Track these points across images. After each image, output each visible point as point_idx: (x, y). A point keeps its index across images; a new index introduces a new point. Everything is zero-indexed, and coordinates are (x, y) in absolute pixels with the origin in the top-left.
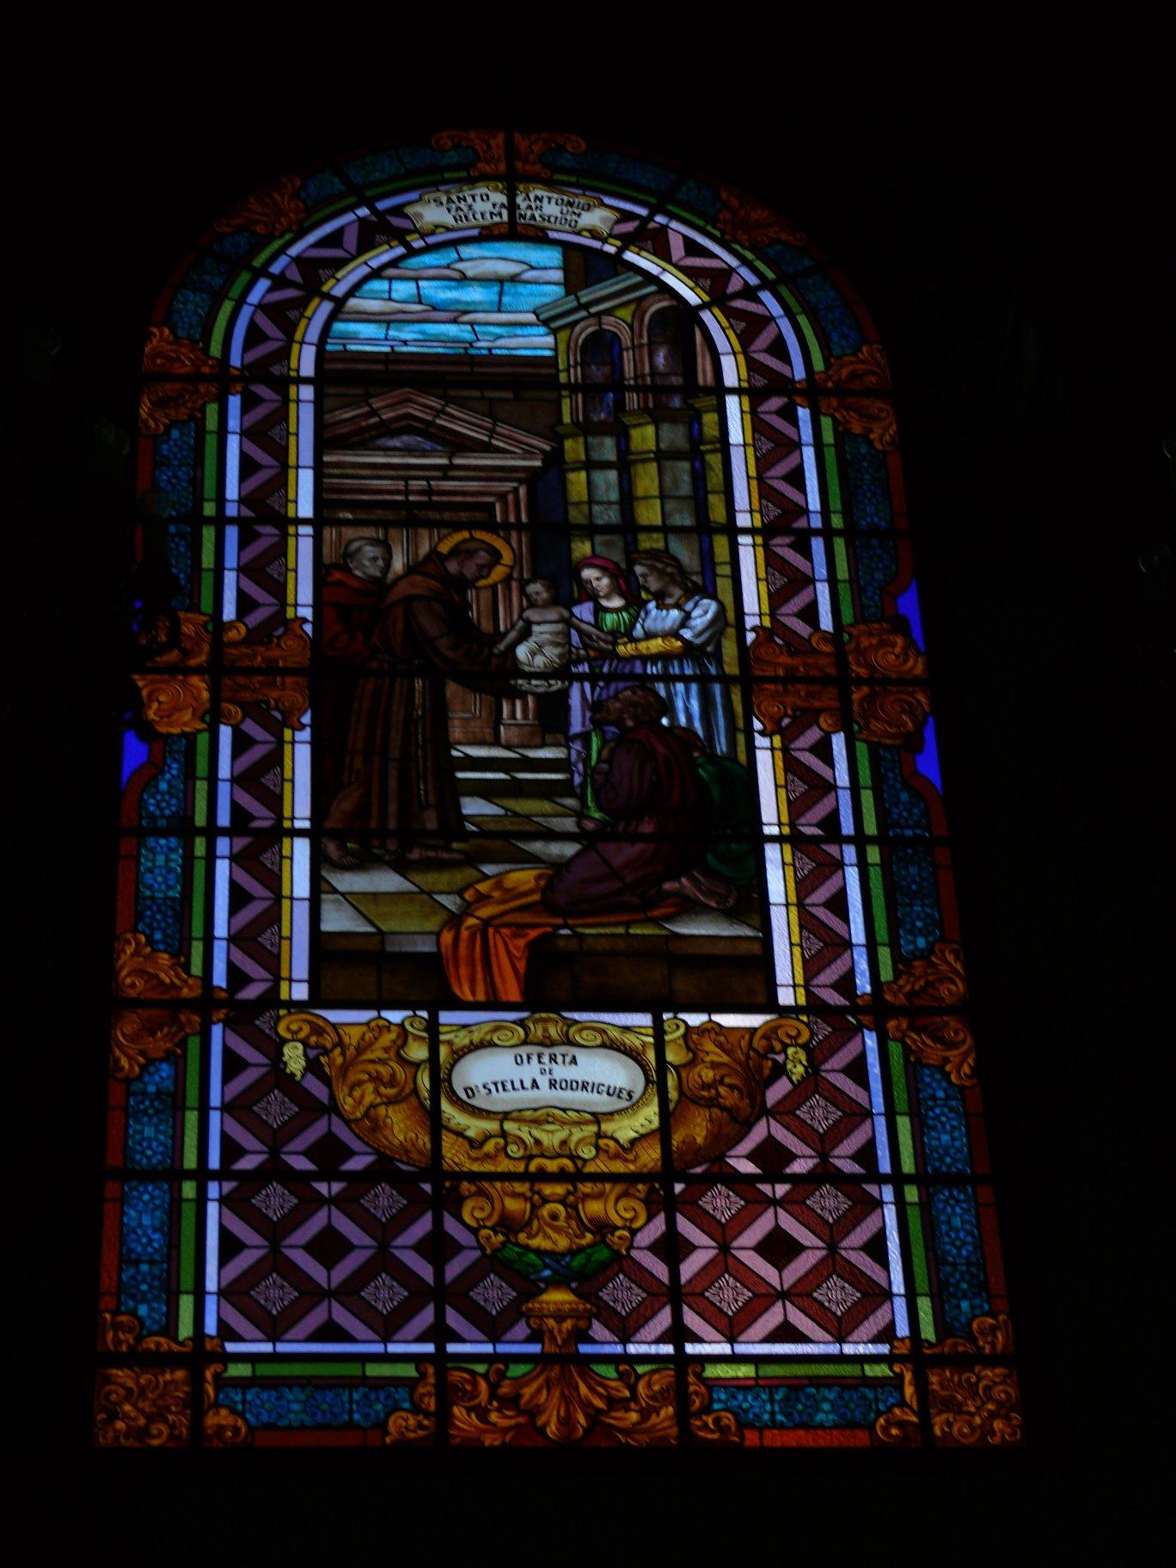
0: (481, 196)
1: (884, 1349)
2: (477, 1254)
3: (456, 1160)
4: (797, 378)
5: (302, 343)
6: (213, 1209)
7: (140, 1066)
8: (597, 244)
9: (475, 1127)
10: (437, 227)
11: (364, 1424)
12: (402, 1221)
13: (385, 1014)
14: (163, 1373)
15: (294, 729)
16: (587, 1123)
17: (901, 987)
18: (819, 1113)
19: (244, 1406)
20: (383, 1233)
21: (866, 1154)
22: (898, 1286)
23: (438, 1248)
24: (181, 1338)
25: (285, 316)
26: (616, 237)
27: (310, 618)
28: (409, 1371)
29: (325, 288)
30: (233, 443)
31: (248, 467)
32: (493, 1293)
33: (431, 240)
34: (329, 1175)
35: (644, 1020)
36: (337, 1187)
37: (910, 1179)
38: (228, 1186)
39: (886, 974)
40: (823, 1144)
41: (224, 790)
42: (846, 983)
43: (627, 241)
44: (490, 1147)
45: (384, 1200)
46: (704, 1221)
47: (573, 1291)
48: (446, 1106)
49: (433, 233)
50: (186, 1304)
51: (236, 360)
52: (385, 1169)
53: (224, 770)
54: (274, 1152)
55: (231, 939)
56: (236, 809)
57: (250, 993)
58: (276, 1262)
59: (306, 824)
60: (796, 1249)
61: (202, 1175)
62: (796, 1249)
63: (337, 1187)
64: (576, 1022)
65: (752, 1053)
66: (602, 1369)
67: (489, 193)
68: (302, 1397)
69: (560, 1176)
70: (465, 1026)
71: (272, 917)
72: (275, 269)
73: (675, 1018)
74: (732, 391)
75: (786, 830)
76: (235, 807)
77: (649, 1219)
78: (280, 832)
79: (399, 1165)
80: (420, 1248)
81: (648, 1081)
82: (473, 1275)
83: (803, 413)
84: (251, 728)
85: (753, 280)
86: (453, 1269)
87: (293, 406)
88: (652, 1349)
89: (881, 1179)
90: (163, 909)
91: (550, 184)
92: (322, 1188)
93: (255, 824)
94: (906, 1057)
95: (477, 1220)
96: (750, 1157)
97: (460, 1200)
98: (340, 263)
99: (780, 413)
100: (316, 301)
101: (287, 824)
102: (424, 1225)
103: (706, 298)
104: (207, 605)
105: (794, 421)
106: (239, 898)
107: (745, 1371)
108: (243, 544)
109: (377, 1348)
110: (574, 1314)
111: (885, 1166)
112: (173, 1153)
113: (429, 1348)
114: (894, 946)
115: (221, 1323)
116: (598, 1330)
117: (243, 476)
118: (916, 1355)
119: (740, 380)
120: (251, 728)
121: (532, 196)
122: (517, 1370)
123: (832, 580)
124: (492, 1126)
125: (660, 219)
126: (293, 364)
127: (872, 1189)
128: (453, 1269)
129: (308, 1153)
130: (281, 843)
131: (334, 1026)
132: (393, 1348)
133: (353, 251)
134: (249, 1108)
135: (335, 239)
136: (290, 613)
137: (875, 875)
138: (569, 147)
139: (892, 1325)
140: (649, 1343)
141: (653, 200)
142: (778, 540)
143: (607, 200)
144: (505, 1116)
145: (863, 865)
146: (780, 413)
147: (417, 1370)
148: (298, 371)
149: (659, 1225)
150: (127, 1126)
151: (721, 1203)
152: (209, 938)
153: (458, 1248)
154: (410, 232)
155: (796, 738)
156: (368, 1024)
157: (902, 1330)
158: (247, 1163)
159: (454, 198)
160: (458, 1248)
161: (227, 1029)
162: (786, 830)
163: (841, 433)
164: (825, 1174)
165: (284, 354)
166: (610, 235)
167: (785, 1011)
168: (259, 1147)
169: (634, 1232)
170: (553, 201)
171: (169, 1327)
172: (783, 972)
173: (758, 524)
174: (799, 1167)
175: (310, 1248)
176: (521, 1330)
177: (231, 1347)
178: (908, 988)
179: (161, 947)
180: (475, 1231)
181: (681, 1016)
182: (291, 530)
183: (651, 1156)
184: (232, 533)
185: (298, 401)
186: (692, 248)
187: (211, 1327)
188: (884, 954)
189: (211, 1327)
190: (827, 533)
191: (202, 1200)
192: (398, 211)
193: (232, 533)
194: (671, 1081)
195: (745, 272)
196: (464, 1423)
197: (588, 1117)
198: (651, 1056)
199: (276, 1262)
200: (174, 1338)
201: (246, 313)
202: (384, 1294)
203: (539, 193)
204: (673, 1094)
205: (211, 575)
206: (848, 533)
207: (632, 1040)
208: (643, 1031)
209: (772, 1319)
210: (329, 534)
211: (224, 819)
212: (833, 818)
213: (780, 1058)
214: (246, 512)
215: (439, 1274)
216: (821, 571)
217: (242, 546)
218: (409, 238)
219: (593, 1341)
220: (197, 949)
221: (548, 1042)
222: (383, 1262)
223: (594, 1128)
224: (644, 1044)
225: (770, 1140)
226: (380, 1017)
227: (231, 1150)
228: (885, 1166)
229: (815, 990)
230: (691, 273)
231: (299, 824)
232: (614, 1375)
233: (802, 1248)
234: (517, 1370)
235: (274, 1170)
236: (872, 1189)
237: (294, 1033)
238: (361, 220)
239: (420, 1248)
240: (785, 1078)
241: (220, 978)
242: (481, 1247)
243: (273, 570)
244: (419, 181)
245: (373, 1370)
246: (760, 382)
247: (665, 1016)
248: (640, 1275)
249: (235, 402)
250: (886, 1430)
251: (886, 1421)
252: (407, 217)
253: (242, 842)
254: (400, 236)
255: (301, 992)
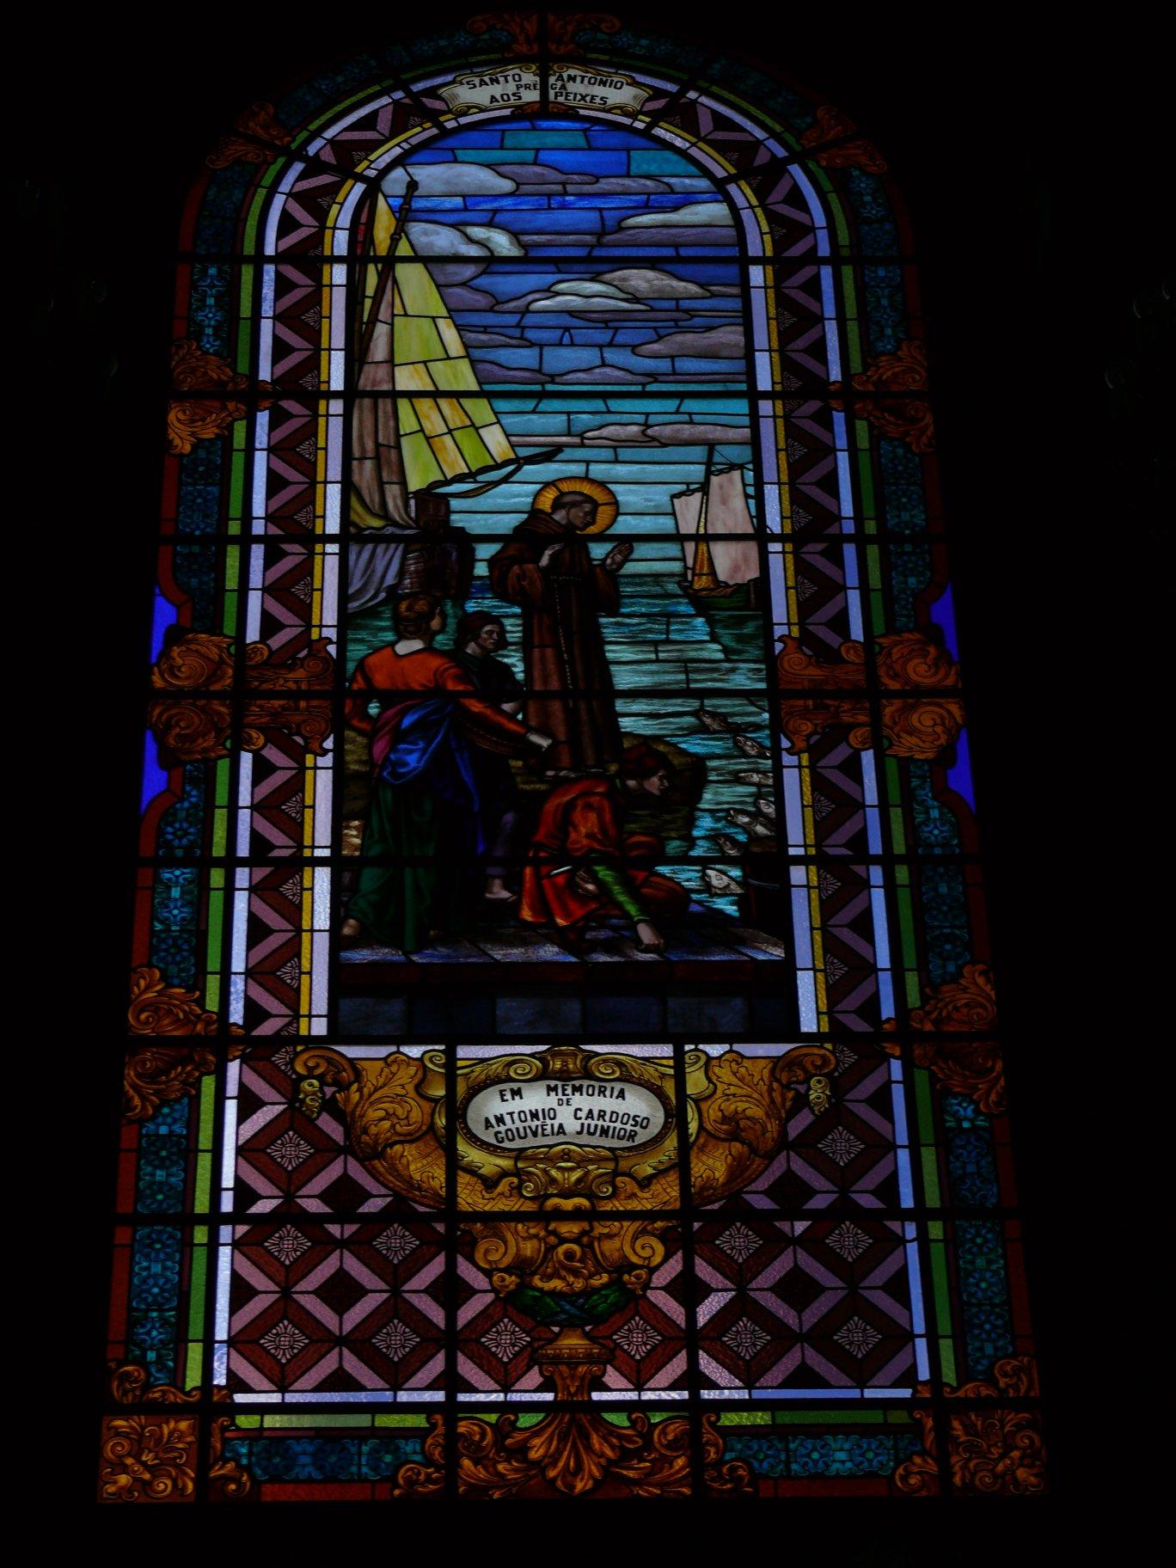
0: (514, 76)
1: (906, 1393)
2: (490, 1297)
3: (470, 1201)
4: (832, 379)
5: (334, 228)
6: (225, 1254)
7: (154, 1108)
8: (627, 121)
9: (489, 1164)
10: (469, 108)
11: (372, 1476)
12: (415, 1264)
13: (405, 1049)
14: (167, 1423)
15: (316, 755)
16: (606, 1159)
17: (869, 377)
18: (849, 1242)
19: (249, 1459)
20: (396, 1276)
21: (889, 1188)
22: (902, 1137)
23: (451, 1291)
24: (188, 1388)
25: (317, 203)
26: (646, 114)
27: (334, 638)
28: (419, 1421)
29: (358, 170)
30: (261, 459)
31: (275, 483)
32: (506, 1340)
33: (463, 120)
34: (339, 1218)
35: (667, 1050)
36: (350, 1229)
37: (901, 859)
38: (242, 1229)
39: (913, 999)
40: (844, 1178)
41: (244, 816)
42: (871, 1008)
43: (656, 117)
44: (503, 1186)
45: (396, 1242)
46: (721, 1263)
47: (586, 1336)
48: (462, 1147)
49: (465, 114)
50: (195, 1352)
51: (265, 373)
52: (400, 1211)
53: (245, 798)
54: (289, 1197)
55: (249, 973)
56: (256, 837)
57: (267, 1029)
58: (286, 1308)
59: (326, 853)
60: (815, 1289)
61: (215, 1219)
62: (815, 1289)
63: (350, 1229)
64: (597, 1054)
65: (775, 1085)
66: (612, 1417)
67: (521, 73)
68: (310, 1449)
69: (576, 1215)
70: (483, 1060)
71: (292, 950)
72: (312, 150)
73: (696, 1050)
74: (766, 395)
75: (812, 851)
76: (255, 836)
77: (667, 1257)
78: (300, 862)
79: (416, 1206)
80: (432, 1290)
81: (667, 1115)
82: (485, 1320)
83: (839, 418)
84: (273, 754)
85: (781, 152)
86: (466, 1313)
87: (322, 421)
88: (664, 1395)
89: (906, 1215)
90: (178, 959)
91: (584, 62)
92: (335, 1229)
93: (276, 853)
94: (932, 1085)
95: (490, 1262)
96: (767, 1193)
97: (473, 1243)
98: (374, 145)
99: (265, 1015)
100: (350, 182)
101: (307, 853)
102: (436, 1267)
103: (733, 171)
104: (230, 627)
105: (829, 426)
106: (257, 931)
107: (761, 1418)
108: (269, 562)
109: (387, 1396)
110: (590, 1359)
111: (907, 1202)
112: (181, 1269)
113: (439, 1396)
114: (922, 968)
115: (231, 1374)
116: (612, 1377)
117: (271, 493)
118: (936, 1400)
119: (773, 383)
120: (273, 754)
121: (565, 76)
122: (526, 1420)
123: (864, 588)
124: (505, 1163)
125: (692, 95)
126: (324, 378)
127: (894, 1226)
128: (466, 1313)
129: (323, 1196)
130: (302, 871)
131: (351, 1061)
132: (403, 1397)
133: (387, 133)
134: (256, 1342)
135: (369, 122)
136: (315, 635)
137: (904, 896)
138: (603, 26)
139: (914, 1367)
140: (664, 1389)
141: (685, 77)
142: (812, 547)
143: (640, 78)
144: (519, 1154)
145: (890, 887)
146: (265, 1015)
147: (428, 1420)
148: (328, 382)
149: (675, 1266)
150: (139, 1169)
151: (738, 1241)
152: (226, 973)
153: (471, 1292)
154: (444, 113)
155: (824, 755)
156: (385, 1059)
157: (924, 1374)
158: (262, 1207)
159: (486, 79)
160: (471, 1292)
161: (244, 1066)
162: (812, 851)
163: (876, 438)
164: (845, 1209)
165: (317, 239)
166: (641, 112)
167: (809, 1037)
168: (278, 1098)
169: (652, 1270)
170: (586, 80)
171: (179, 1375)
172: (779, 612)
173: (788, 530)
174: (819, 1202)
175: (322, 1292)
176: (534, 1377)
177: (240, 1398)
178: (875, 378)
179: (176, 981)
180: (488, 1274)
181: (701, 1047)
182: (318, 548)
183: (667, 1193)
184: (257, 552)
185: (327, 415)
186: (721, 122)
187: (220, 1379)
188: (912, 980)
189: (220, 1379)
190: (860, 539)
191: (213, 1246)
192: (432, 93)
193: (257, 552)
194: (692, 1114)
195: (773, 144)
196: (472, 1478)
197: (607, 1153)
198: (670, 1088)
199: (286, 1308)
200: (182, 1389)
201: (279, 202)
202: (396, 1340)
203: (572, 72)
204: (693, 1127)
205: (941, 1332)
206: (882, 538)
207: (650, 1072)
208: (665, 1062)
209: (789, 1363)
210: (360, 557)
211: (243, 850)
212: (861, 837)
213: (802, 1089)
214: (274, 530)
215: (451, 1318)
216: (852, 578)
217: (268, 565)
218: (442, 119)
219: (606, 1388)
220: (213, 983)
221: (564, 1076)
222: (397, 1308)
223: (611, 1165)
224: (663, 1076)
225: (789, 1174)
226: (398, 1052)
227: (244, 1193)
228: (907, 1202)
229: (839, 1016)
230: (721, 147)
231: (318, 853)
232: (626, 1424)
233: (823, 1289)
234: (526, 1420)
235: (288, 1214)
236: (894, 1226)
237: (310, 1070)
238: (396, 103)
239: (432, 1290)
240: (806, 1111)
241: (237, 1014)
242: (494, 1290)
243: (289, 808)
244: (453, 63)
245: (384, 1421)
246: (796, 384)
247: (687, 1047)
248: (657, 1317)
249: (263, 418)
250: (904, 1478)
251: (905, 1469)
252: (440, 98)
253: (262, 873)
254: (433, 116)
255: (320, 1028)
